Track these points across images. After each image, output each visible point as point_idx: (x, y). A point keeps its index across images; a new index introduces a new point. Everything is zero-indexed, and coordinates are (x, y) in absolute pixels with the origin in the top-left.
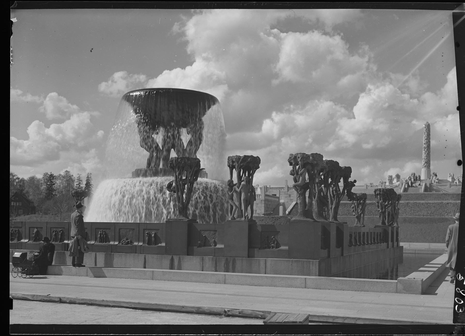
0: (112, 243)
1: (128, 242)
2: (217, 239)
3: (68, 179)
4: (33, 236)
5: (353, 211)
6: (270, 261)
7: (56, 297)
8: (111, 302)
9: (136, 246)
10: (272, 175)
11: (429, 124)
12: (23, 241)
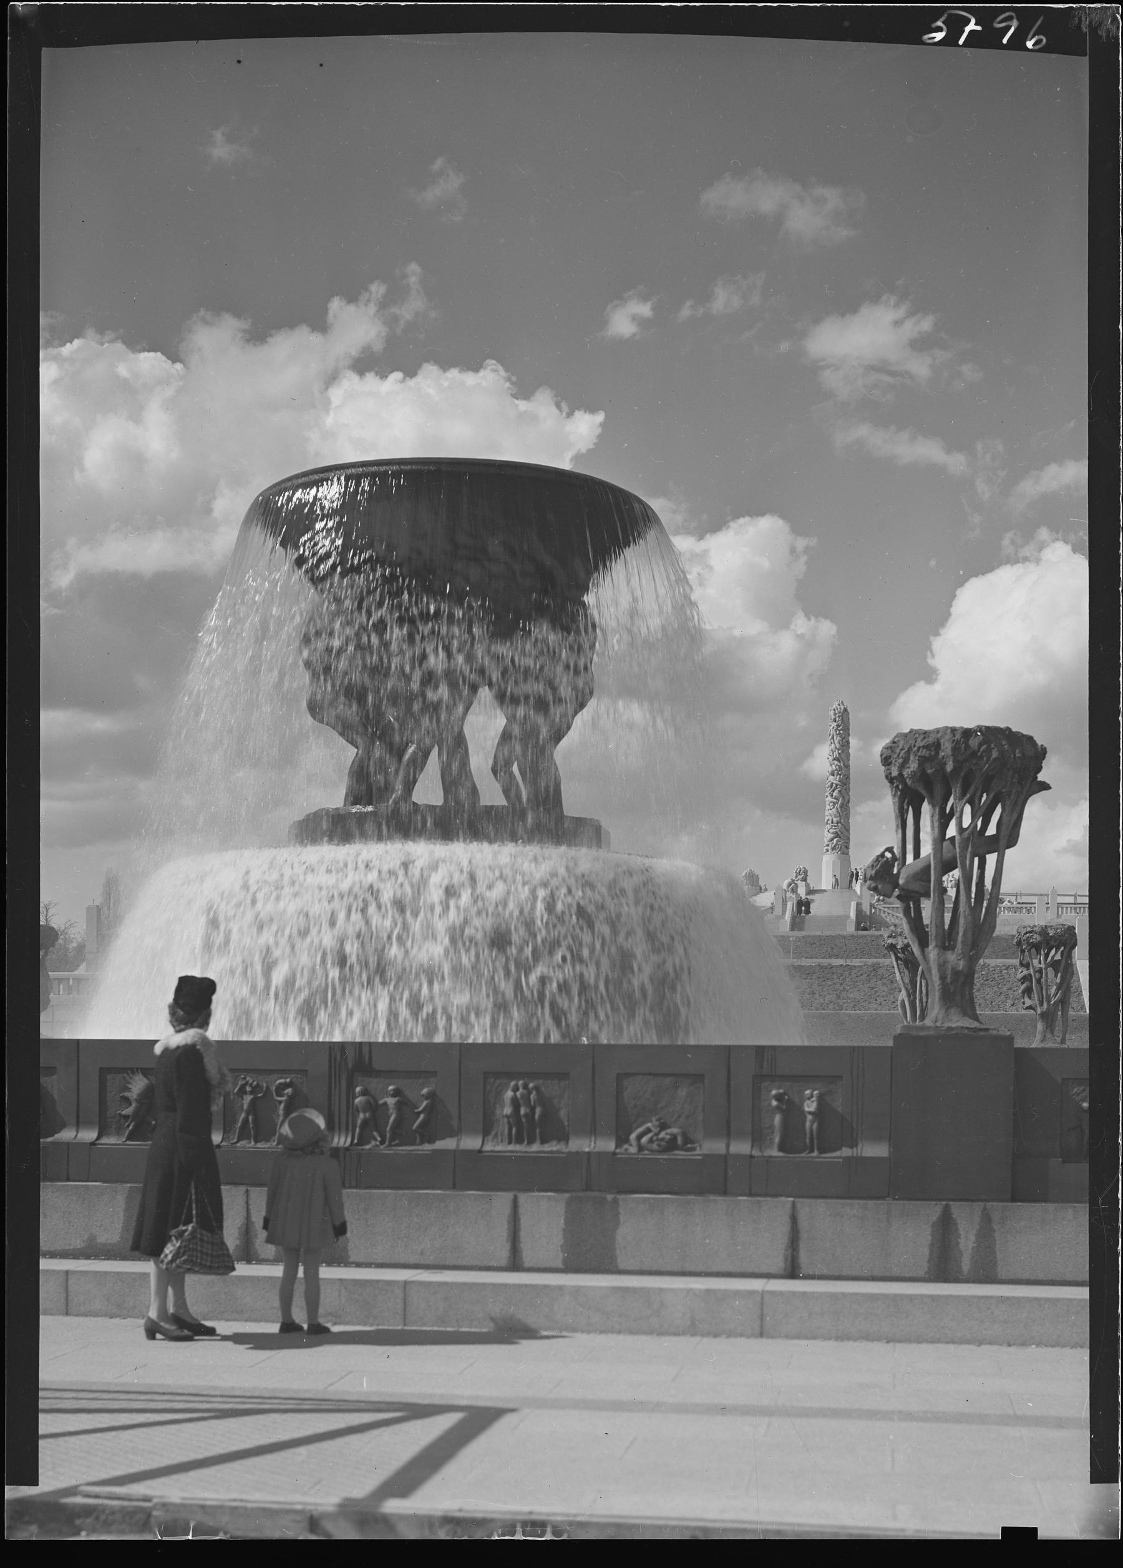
0: (581, 1144)
1: (674, 1138)
9: (68, 1145)
11: (845, 710)
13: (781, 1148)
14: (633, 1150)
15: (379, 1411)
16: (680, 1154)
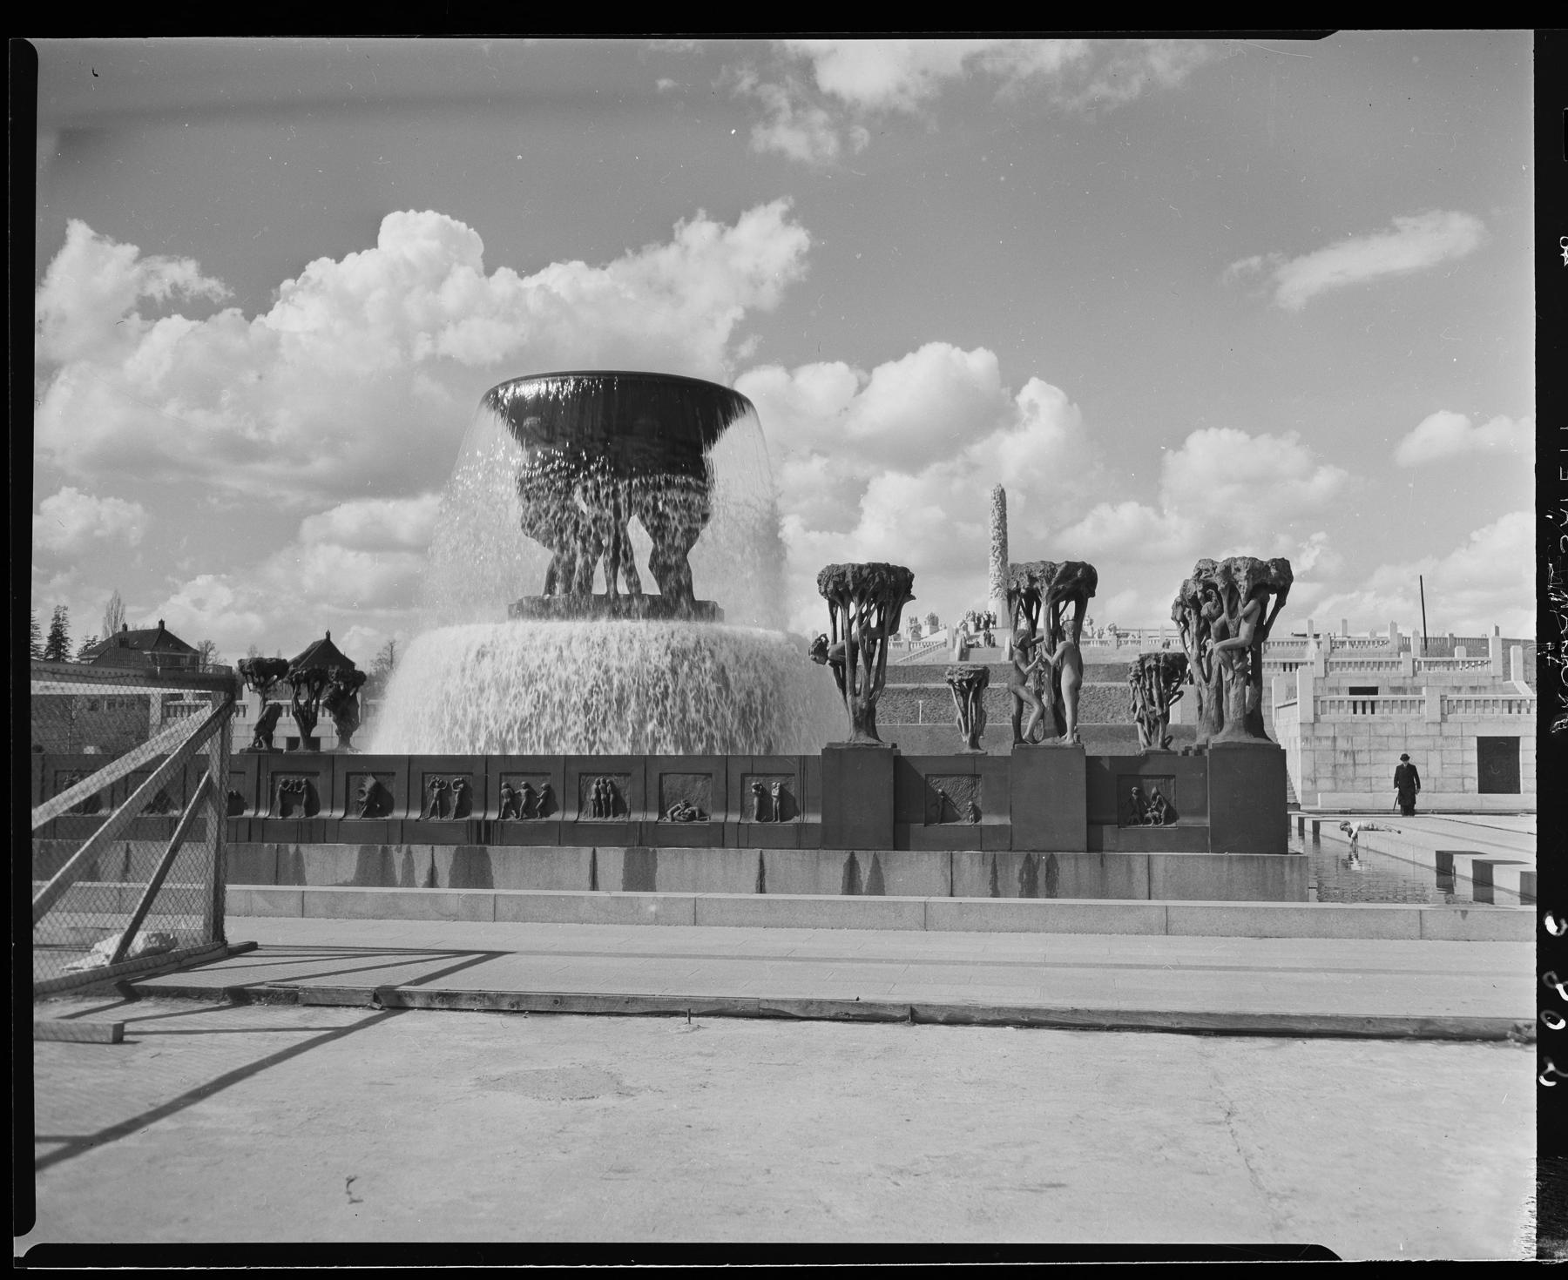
0: (637, 817)
4: (364, 799)
6: (1161, 859)
7: (894, 1006)
8: (1104, 1013)
12: (324, 814)
15: (332, 957)
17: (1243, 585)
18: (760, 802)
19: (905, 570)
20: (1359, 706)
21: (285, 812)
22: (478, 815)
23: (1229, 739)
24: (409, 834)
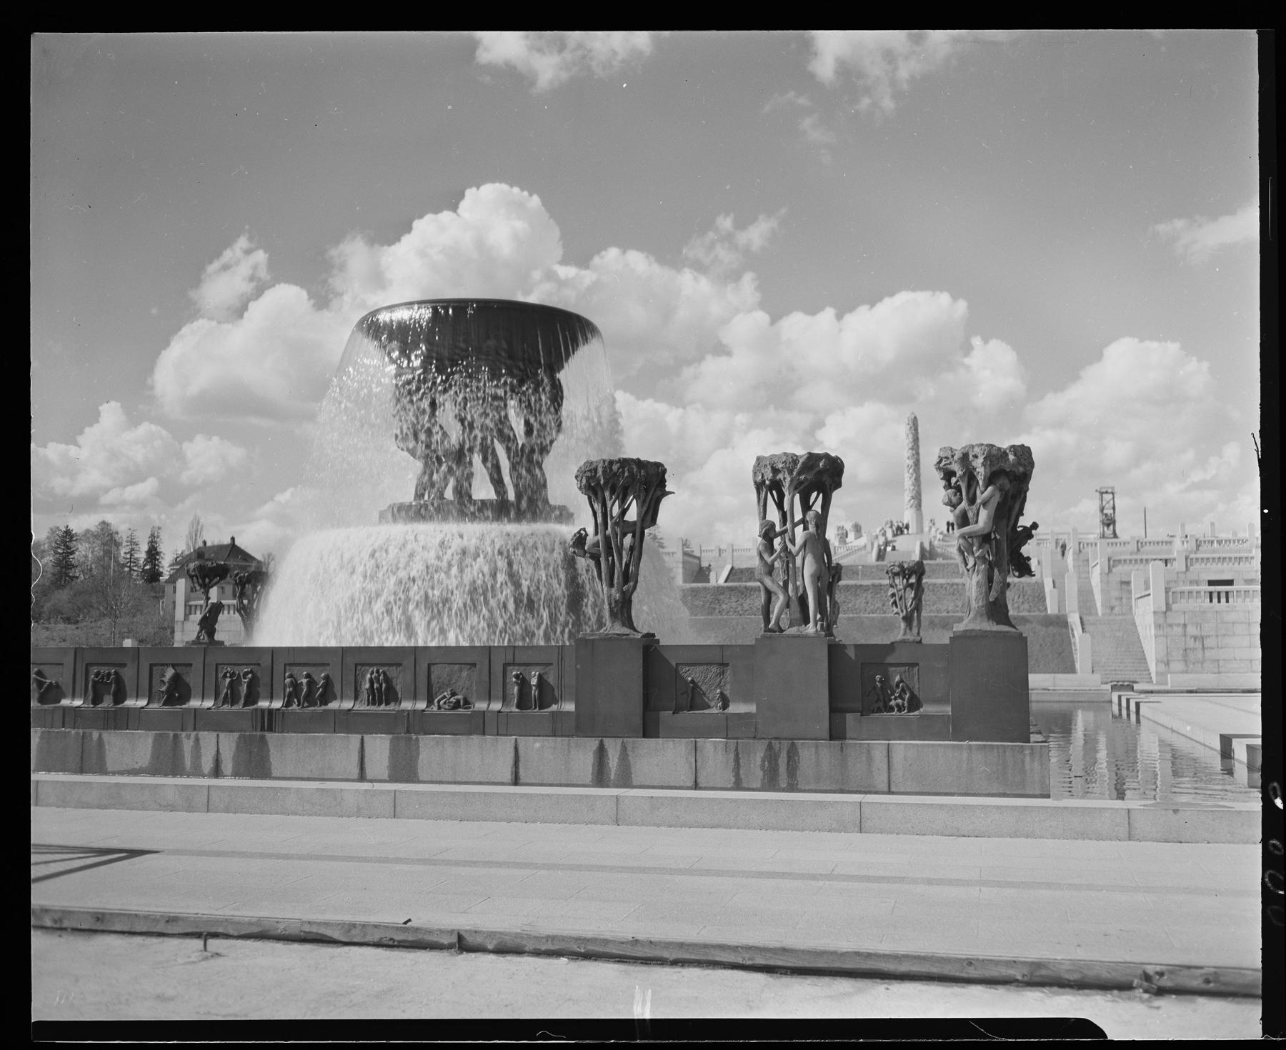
0: (407, 705)
1: (458, 701)
2: (728, 686)
3: (107, 537)
4: (164, 689)
5: (895, 603)
6: (901, 747)
7: (441, 931)
8: (668, 945)
10: (714, 516)
12: (130, 703)
13: (518, 707)
14: (435, 708)
16: (461, 710)
17: (981, 472)
18: (520, 691)
19: (658, 465)
20: (1215, 596)
21: (96, 700)
22: (264, 704)
23: (971, 627)
24: (200, 721)
